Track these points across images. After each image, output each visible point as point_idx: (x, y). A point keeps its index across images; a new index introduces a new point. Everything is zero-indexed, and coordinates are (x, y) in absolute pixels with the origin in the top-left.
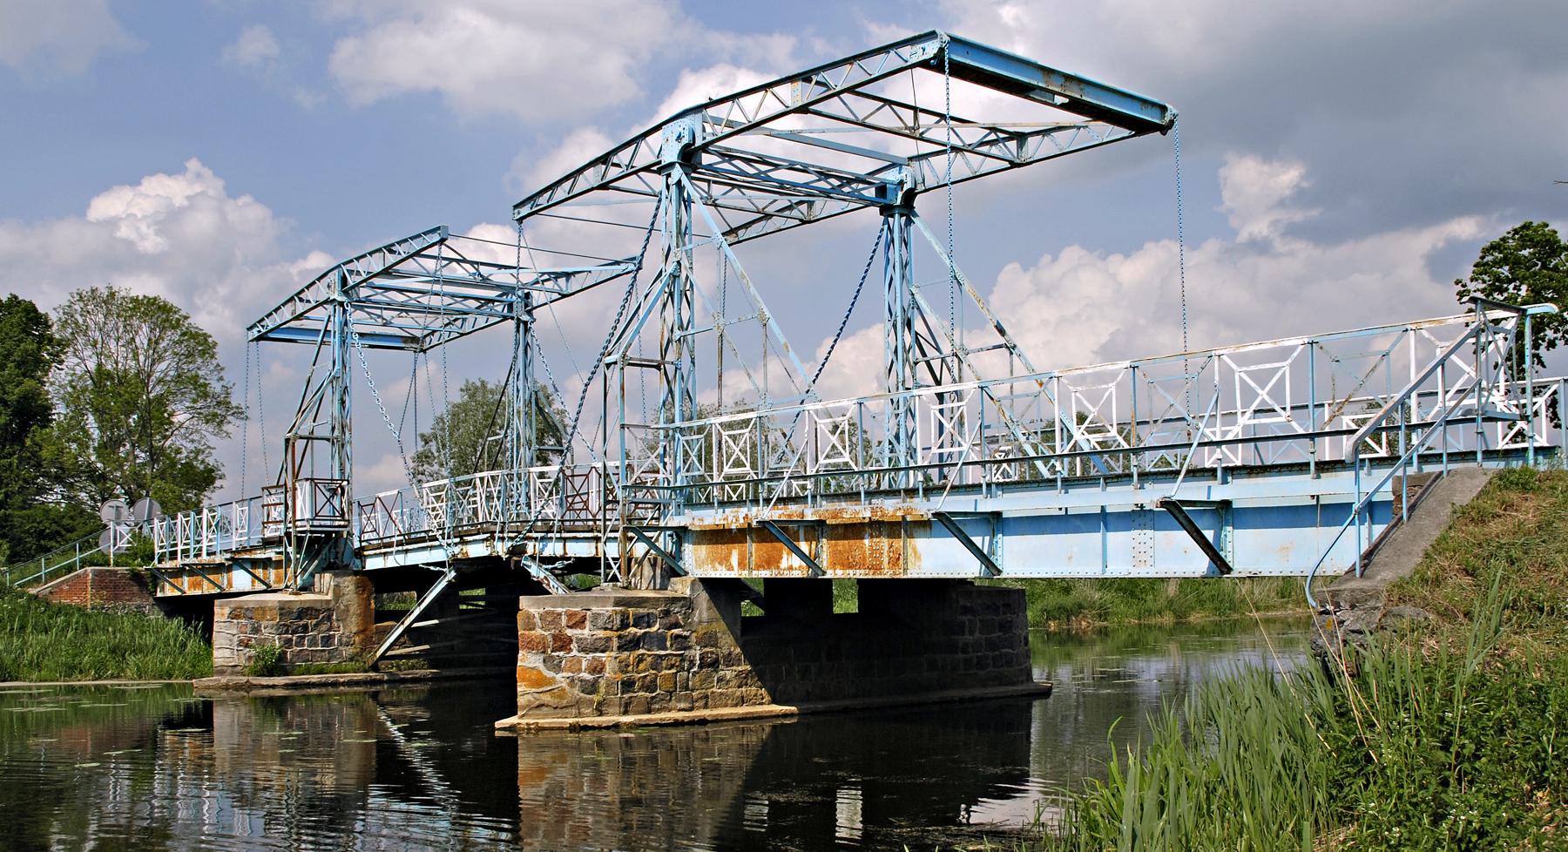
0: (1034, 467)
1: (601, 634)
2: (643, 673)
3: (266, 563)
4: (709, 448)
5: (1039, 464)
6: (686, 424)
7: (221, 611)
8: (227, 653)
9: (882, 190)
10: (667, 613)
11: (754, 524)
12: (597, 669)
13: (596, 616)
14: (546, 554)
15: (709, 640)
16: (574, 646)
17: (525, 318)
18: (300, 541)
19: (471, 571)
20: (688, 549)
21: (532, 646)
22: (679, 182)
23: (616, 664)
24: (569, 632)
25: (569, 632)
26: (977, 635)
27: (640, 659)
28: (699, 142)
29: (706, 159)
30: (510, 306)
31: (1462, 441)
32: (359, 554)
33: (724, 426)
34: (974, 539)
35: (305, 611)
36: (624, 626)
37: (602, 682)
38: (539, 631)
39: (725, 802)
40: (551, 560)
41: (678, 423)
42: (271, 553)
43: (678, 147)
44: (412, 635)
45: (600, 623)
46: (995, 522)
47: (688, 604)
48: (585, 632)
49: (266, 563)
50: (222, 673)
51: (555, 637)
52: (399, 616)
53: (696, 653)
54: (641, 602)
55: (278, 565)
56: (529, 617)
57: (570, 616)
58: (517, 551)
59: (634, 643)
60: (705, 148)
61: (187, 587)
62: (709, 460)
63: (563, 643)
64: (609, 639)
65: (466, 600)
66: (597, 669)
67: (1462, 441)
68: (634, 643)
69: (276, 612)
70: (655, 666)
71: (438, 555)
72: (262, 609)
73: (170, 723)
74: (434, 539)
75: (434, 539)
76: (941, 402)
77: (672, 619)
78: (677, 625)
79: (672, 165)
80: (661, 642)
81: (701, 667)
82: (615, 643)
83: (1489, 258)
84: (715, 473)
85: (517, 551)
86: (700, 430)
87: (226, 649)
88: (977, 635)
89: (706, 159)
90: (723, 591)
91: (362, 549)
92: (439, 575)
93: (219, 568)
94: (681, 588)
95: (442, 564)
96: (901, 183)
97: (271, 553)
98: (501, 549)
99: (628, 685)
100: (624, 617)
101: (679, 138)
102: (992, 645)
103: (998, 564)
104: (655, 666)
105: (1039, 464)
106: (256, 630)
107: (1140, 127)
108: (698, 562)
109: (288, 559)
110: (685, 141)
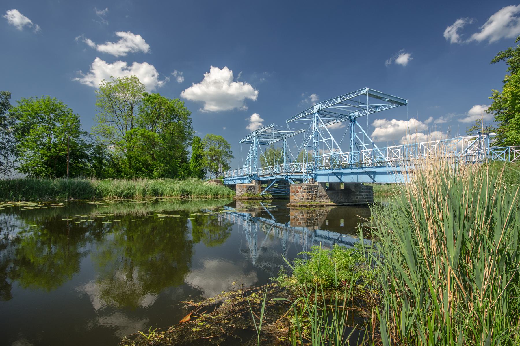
0: (377, 164)
3: (243, 179)
4: (322, 160)
5: (378, 164)
7: (237, 186)
9: (350, 117)
10: (314, 188)
12: (303, 196)
18: (249, 176)
19: (278, 181)
20: (318, 177)
21: (292, 192)
22: (317, 116)
27: (310, 195)
28: (320, 109)
29: (321, 112)
31: (269, 212)
32: (259, 177)
35: (250, 187)
36: (308, 189)
38: (294, 190)
39: (323, 221)
44: (268, 191)
47: (318, 186)
48: (301, 190)
49: (243, 179)
53: (319, 194)
54: (310, 186)
55: (246, 179)
56: (292, 187)
57: (299, 187)
58: (287, 177)
59: (309, 192)
60: (321, 110)
61: (231, 183)
62: (322, 162)
63: (298, 192)
65: (275, 185)
66: (303, 196)
67: (269, 212)
68: (309, 192)
70: (312, 196)
71: (273, 178)
72: (244, 186)
73: (225, 205)
74: (271, 175)
75: (271, 175)
79: (315, 113)
82: (306, 192)
84: (323, 164)
85: (287, 177)
86: (320, 157)
87: (238, 193)
90: (323, 184)
92: (272, 181)
94: (316, 183)
96: (354, 116)
97: (245, 177)
98: (284, 177)
99: (308, 199)
100: (308, 188)
102: (367, 195)
105: (378, 164)
106: (243, 189)
107: (401, 104)
108: (320, 179)
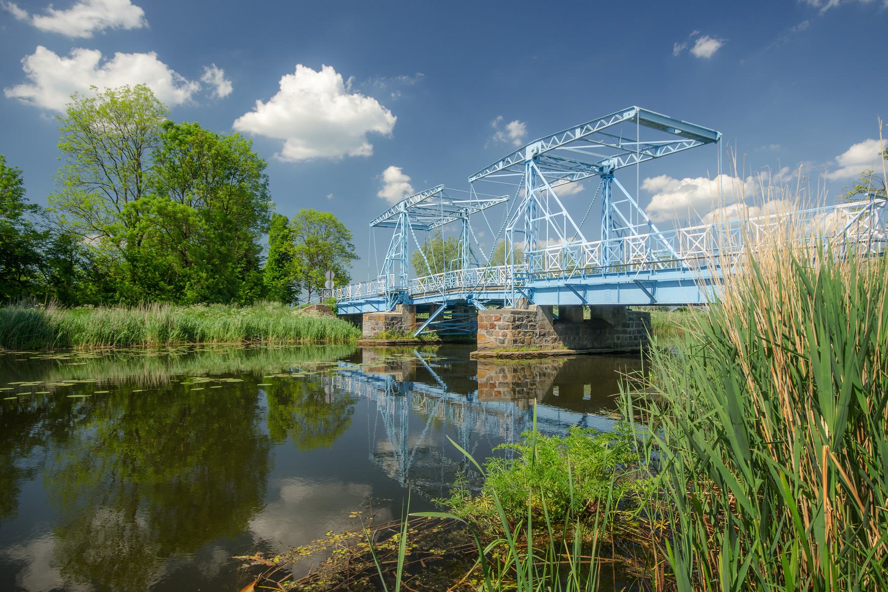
1: (507, 323)
2: (521, 337)
3: (379, 302)
6: (534, 252)
7: (365, 318)
8: (367, 332)
10: (528, 317)
11: (259, 397)
12: (505, 335)
13: (505, 317)
14: (480, 298)
15: (542, 327)
16: (497, 327)
17: (466, 218)
18: (391, 295)
21: (482, 327)
22: (532, 167)
23: (511, 334)
24: (495, 323)
25: (495, 323)
26: (634, 328)
27: (519, 332)
28: (540, 152)
29: (541, 159)
30: (461, 214)
33: (550, 252)
34: (647, 289)
35: (393, 318)
36: (514, 321)
37: (507, 340)
38: (485, 322)
40: (482, 300)
41: (531, 251)
42: (381, 299)
43: (532, 154)
44: (430, 327)
45: (506, 320)
46: (655, 284)
47: (536, 314)
48: (501, 323)
49: (379, 302)
50: (366, 338)
51: (491, 325)
52: (425, 320)
53: (537, 331)
54: (519, 313)
55: (383, 302)
57: (496, 317)
58: (470, 297)
59: (518, 327)
60: (541, 155)
61: (351, 311)
64: (509, 325)
66: (505, 335)
68: (518, 327)
69: (384, 318)
70: (524, 335)
71: (441, 299)
72: (379, 317)
76: (266, 349)
77: (530, 319)
78: (531, 321)
79: (530, 161)
80: (526, 327)
81: (540, 336)
82: (511, 327)
83: (635, 443)
85: (470, 297)
86: (539, 254)
88: (634, 328)
89: (541, 159)
91: (412, 295)
93: (361, 304)
94: (532, 308)
95: (442, 302)
98: (464, 297)
99: (515, 341)
100: (514, 318)
101: (533, 151)
103: (656, 299)
104: (524, 335)
106: (377, 324)
107: (706, 141)
108: (541, 299)
109: (387, 301)
110: (535, 152)
